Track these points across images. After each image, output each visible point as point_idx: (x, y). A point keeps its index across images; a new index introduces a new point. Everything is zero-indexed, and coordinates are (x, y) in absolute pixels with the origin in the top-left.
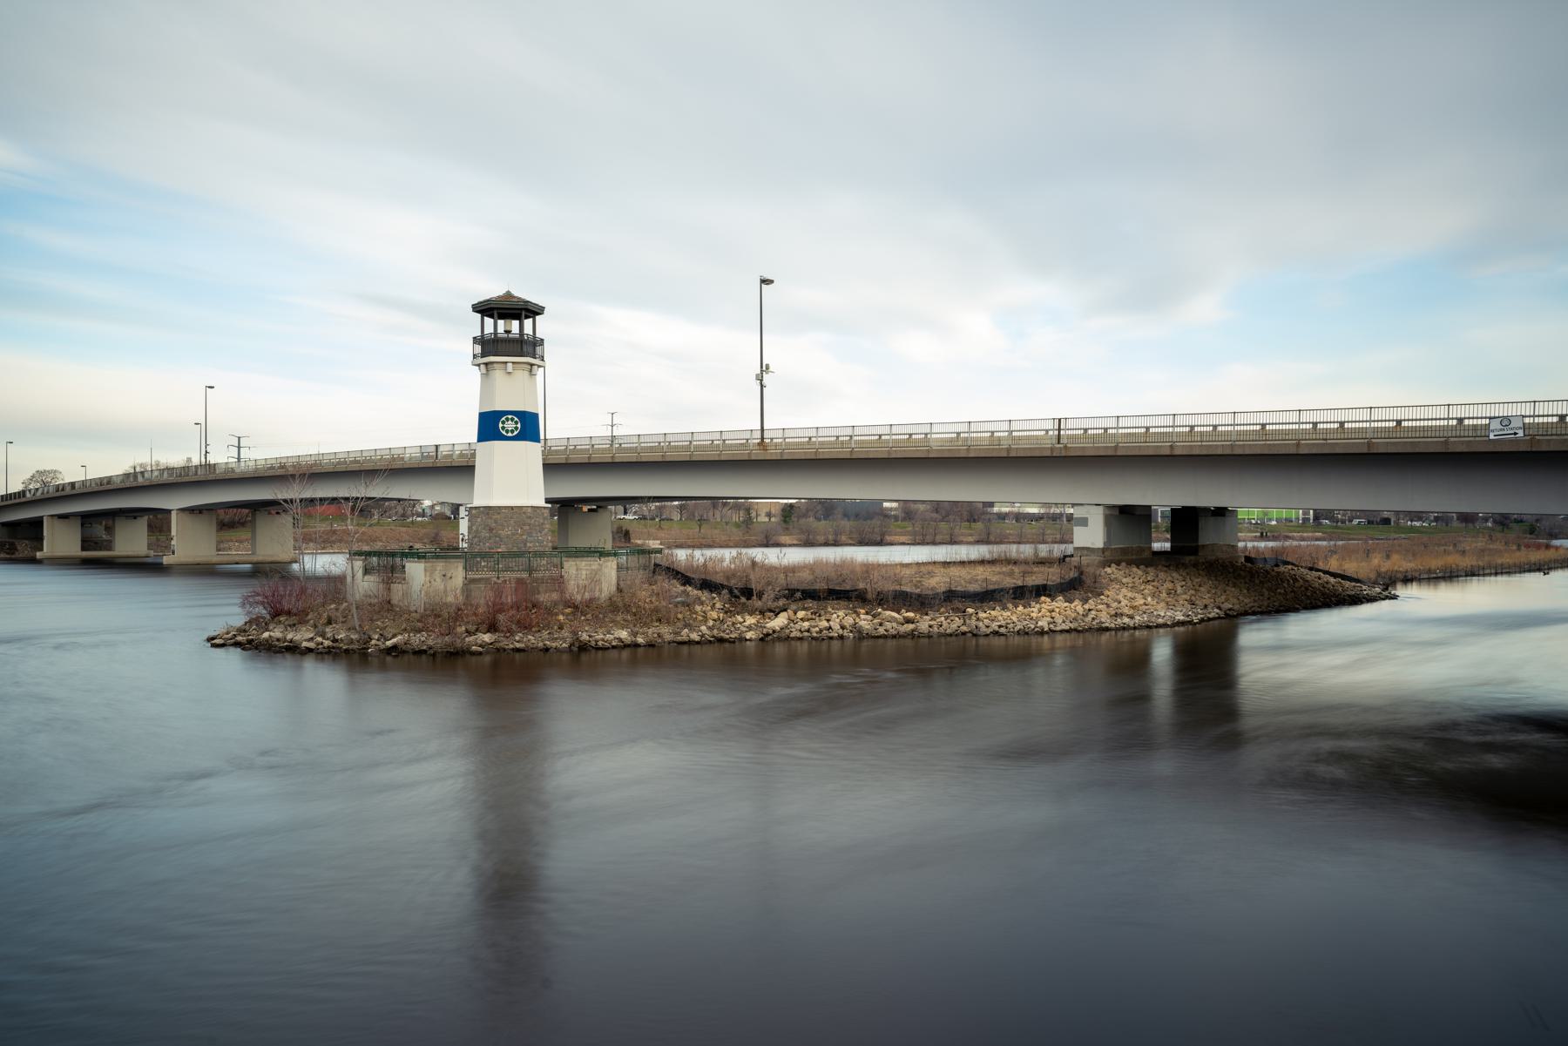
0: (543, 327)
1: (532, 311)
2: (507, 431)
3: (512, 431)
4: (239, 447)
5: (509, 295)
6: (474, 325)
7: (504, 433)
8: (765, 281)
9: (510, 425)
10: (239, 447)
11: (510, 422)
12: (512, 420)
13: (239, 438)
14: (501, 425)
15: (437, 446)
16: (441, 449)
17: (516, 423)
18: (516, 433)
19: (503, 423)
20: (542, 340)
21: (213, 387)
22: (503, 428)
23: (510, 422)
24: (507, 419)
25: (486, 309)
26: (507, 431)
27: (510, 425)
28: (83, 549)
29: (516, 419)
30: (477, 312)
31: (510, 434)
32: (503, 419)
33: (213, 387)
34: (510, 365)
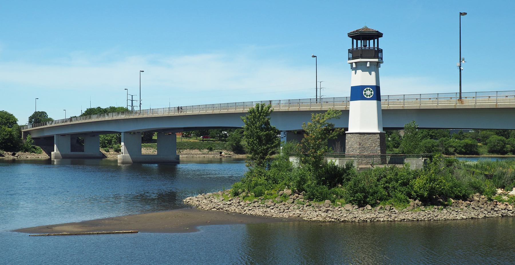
0: (383, 44)
1: (377, 35)
2: (367, 96)
3: (369, 96)
4: (132, 101)
5: (366, 28)
6: (348, 43)
7: (365, 96)
8: (461, 14)
9: (368, 93)
10: (132, 101)
11: (368, 91)
12: (369, 90)
13: (132, 96)
14: (364, 93)
15: (270, 101)
16: (273, 102)
17: (371, 91)
18: (371, 96)
19: (365, 91)
20: (382, 50)
21: (143, 71)
22: (365, 94)
23: (368, 91)
24: (367, 90)
25: (356, 36)
26: (367, 96)
27: (368, 93)
28: (72, 151)
29: (371, 89)
30: (350, 37)
31: (368, 97)
32: (365, 89)
33: (143, 71)
34: (368, 63)
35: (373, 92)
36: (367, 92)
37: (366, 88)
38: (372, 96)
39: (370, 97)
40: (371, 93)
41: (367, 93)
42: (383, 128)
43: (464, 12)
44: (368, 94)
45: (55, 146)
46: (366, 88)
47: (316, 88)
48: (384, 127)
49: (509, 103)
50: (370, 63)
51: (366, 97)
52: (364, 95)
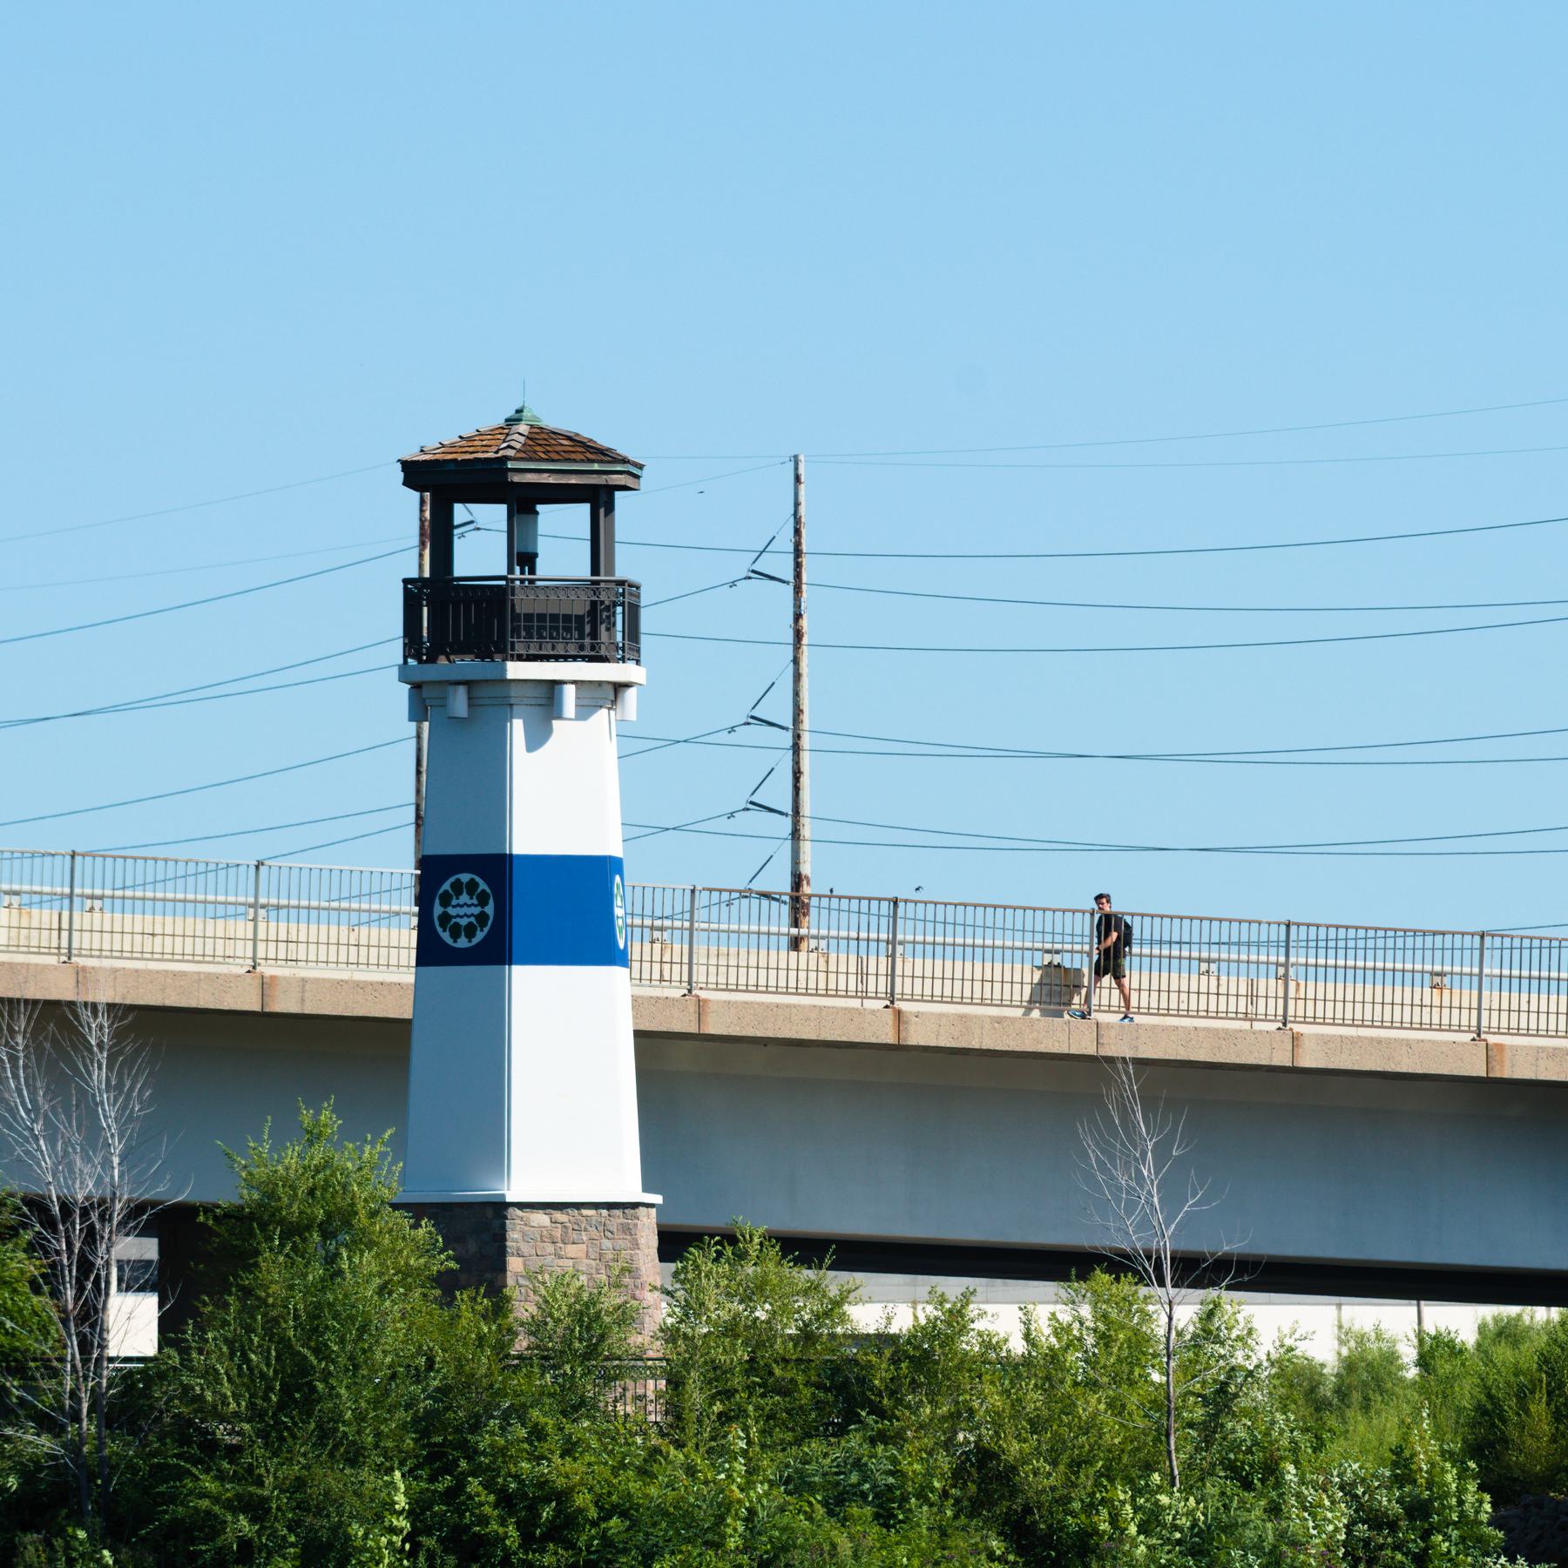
11: (464, 898)
23: (464, 898)
26: (455, 934)
35: (491, 902)
36: (454, 902)
37: (452, 879)
38: (486, 930)
39: (476, 940)
40: (477, 910)
41: (461, 911)
42: (638, 1034)
43: (540, 551)
44: (464, 922)
45: (425, 610)
46: (452, 879)
47: (805, 560)
48: (642, 1027)
49: (856, 1003)
50: (577, 689)
51: (449, 941)
52: (439, 930)
